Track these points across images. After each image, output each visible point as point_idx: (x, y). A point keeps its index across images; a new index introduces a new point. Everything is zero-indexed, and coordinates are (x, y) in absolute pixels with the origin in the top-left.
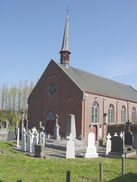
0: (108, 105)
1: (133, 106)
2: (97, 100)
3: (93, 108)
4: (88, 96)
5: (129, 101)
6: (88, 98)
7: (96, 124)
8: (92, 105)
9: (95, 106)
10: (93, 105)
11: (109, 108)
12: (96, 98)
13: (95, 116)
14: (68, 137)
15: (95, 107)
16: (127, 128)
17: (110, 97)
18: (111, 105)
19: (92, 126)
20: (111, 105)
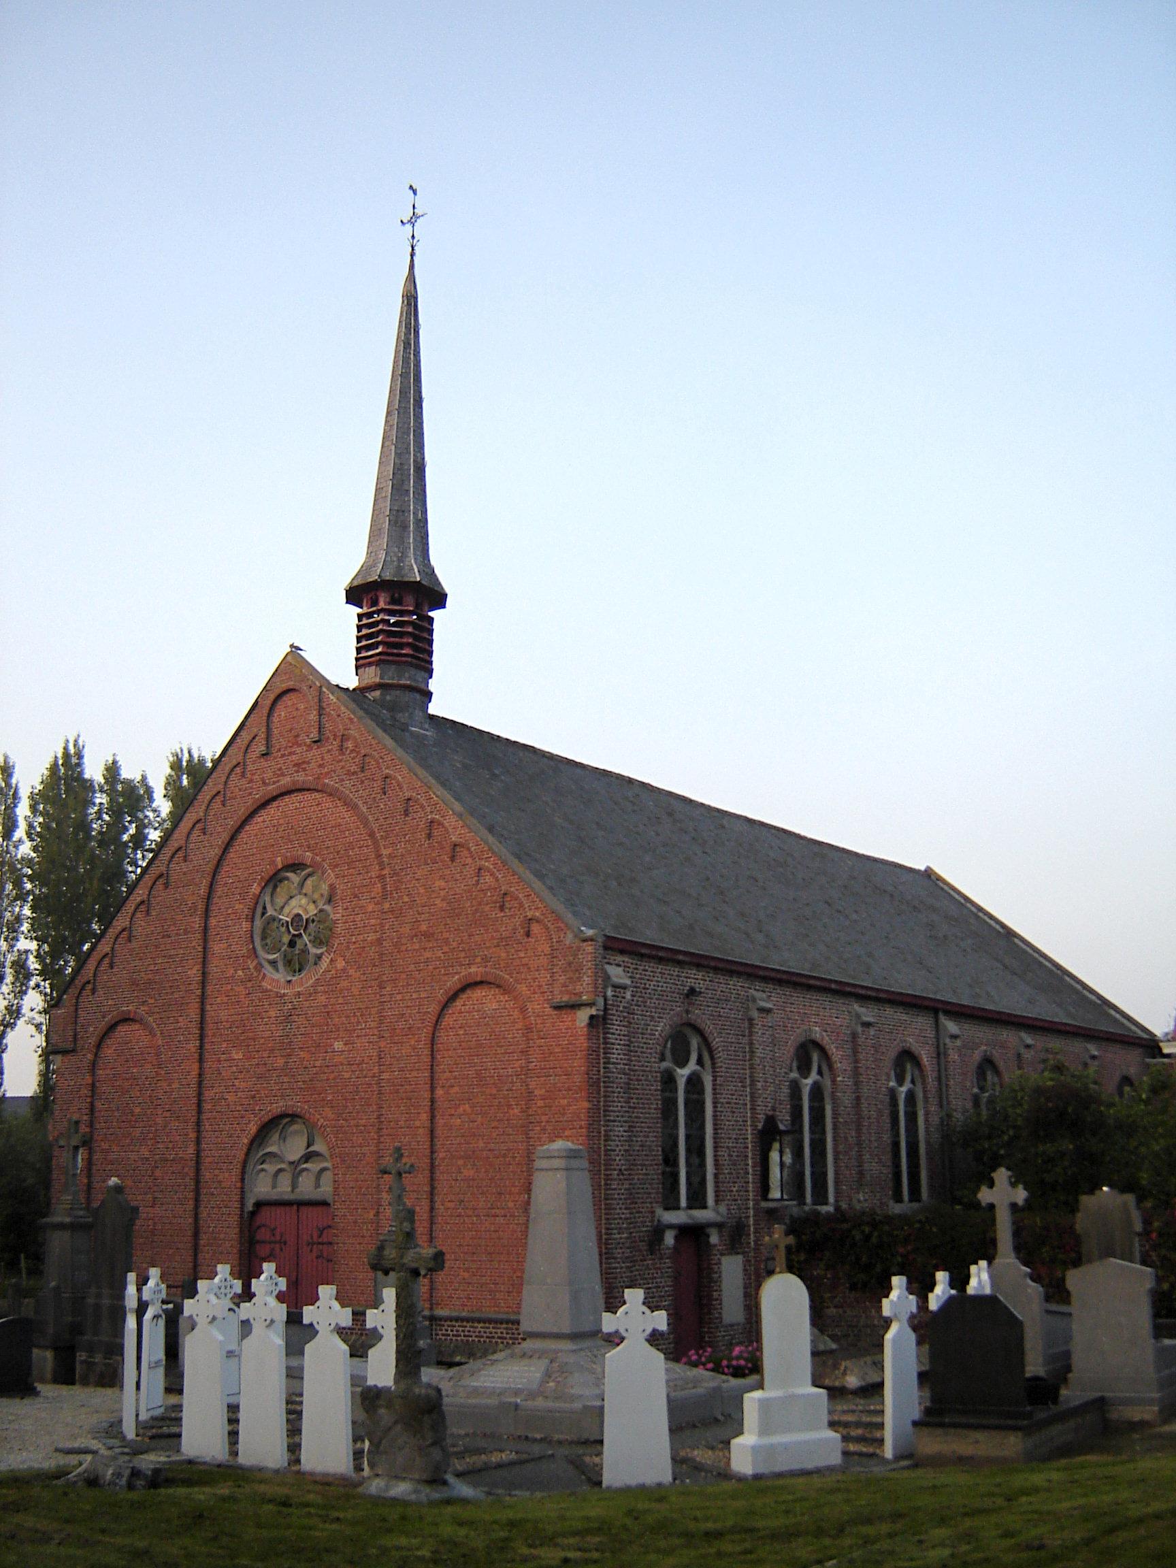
0: (787, 1052)
1: (977, 1056)
2: (700, 1015)
3: (669, 1080)
4: (628, 982)
5: (948, 1013)
6: (628, 995)
7: (701, 1215)
8: (663, 1059)
9: (683, 1063)
10: (668, 1054)
11: (794, 1075)
12: (692, 991)
13: (688, 1150)
14: (11, 764)
15: (683, 1073)
16: (407, 449)
17: (795, 985)
18: (807, 1053)
19: (669, 1239)
20: (807, 1053)
